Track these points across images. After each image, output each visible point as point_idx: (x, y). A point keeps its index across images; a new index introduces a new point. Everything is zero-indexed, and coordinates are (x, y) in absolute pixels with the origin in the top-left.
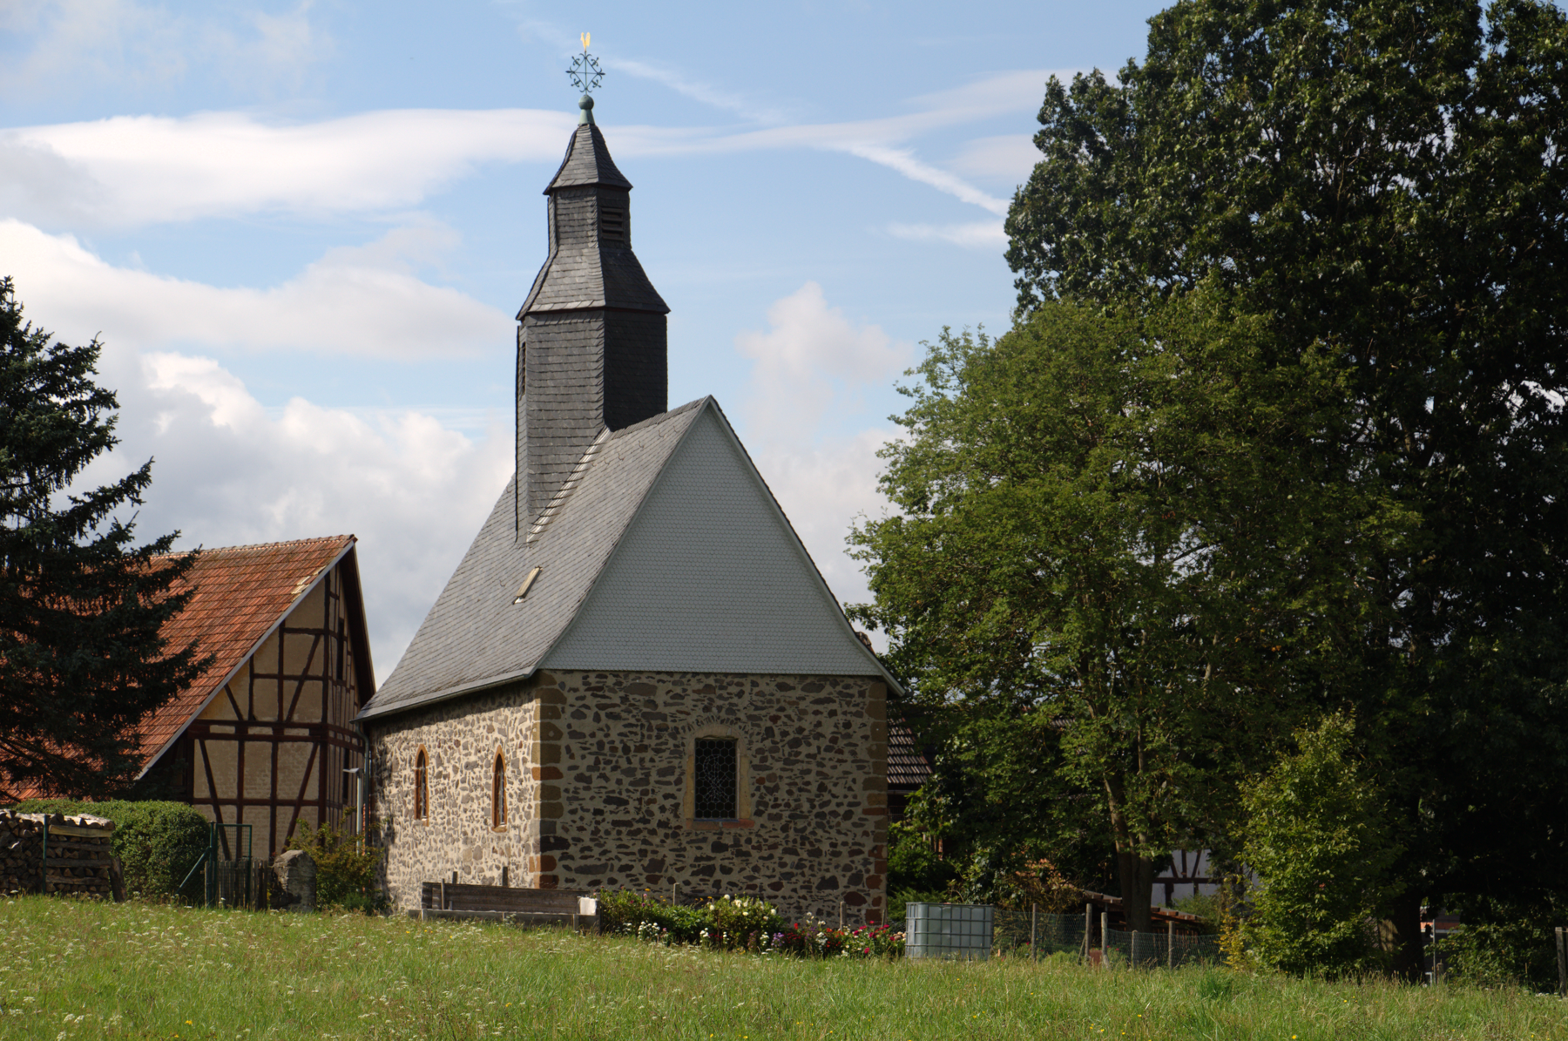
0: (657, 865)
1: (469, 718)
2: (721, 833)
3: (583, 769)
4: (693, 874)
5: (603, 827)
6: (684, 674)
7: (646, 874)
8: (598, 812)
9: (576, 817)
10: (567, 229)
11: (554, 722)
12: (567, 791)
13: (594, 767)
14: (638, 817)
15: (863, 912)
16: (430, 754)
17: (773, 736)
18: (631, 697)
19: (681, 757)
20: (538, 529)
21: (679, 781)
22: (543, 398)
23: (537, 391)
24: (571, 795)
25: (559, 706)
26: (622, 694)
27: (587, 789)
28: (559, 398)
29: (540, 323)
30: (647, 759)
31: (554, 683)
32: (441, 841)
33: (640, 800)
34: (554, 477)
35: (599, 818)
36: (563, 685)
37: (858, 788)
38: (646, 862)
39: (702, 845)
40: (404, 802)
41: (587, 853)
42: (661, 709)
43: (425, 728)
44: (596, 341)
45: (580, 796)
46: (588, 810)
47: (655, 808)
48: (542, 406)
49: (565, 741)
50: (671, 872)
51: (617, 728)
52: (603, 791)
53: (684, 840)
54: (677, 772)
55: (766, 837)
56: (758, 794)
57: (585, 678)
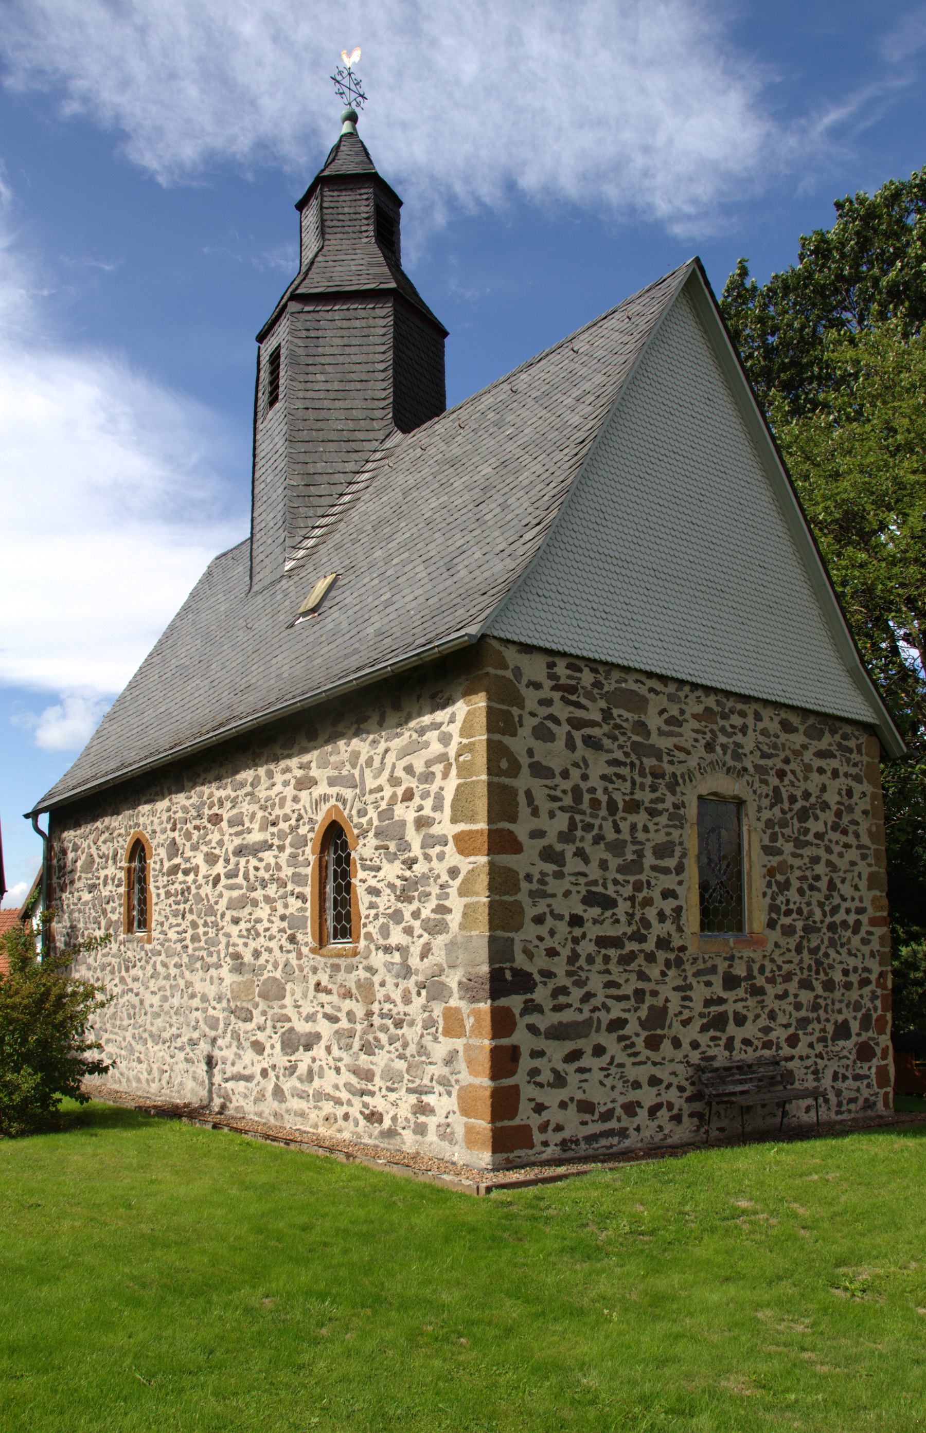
0: (658, 1017)
1: (246, 775)
2: (732, 958)
3: (551, 838)
4: (704, 1029)
5: (587, 948)
6: (681, 682)
7: (644, 1034)
8: (576, 921)
9: (543, 930)
10: (335, 223)
11: (507, 740)
12: (529, 877)
13: (566, 837)
14: (629, 931)
15: (873, 1070)
16: (154, 843)
17: (782, 802)
18: (615, 712)
19: (682, 827)
20: (301, 553)
21: (680, 869)
22: (310, 394)
23: (301, 386)
24: (535, 886)
25: (515, 711)
26: (603, 704)
27: (559, 875)
28: (332, 395)
29: (307, 309)
30: (640, 826)
31: (505, 666)
32: (178, 966)
33: (632, 899)
34: (323, 489)
35: (577, 932)
36: (517, 671)
37: (863, 885)
38: (643, 1013)
39: (711, 978)
40: (104, 912)
41: (562, 999)
42: (655, 740)
43: (145, 808)
44: (383, 331)
45: (549, 889)
46: (560, 917)
47: (651, 913)
48: (308, 404)
49: (523, 782)
50: (676, 1028)
51: (598, 767)
52: (582, 880)
53: (690, 969)
54: (678, 851)
55: (780, 963)
56: (769, 892)
57: (551, 666)
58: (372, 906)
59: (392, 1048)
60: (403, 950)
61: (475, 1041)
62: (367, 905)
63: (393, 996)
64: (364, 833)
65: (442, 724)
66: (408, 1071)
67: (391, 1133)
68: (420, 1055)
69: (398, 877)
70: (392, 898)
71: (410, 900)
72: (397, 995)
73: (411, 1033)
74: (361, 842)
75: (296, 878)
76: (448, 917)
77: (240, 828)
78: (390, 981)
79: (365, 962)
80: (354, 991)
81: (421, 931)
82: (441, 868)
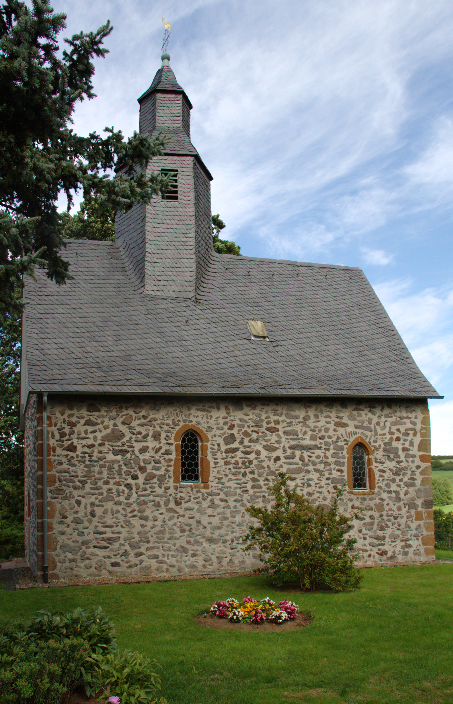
58: (381, 476)
59: (393, 527)
60: (397, 493)
61: (427, 521)
62: (378, 475)
63: (393, 508)
64: (377, 449)
65: (411, 418)
66: (401, 534)
67: (392, 557)
68: (406, 527)
69: (266, 457)
70: (391, 474)
71: (399, 475)
72: (395, 508)
73: (402, 521)
74: (376, 452)
75: (337, 463)
76: (416, 482)
77: (295, 437)
78: (391, 503)
79: (379, 497)
80: (374, 507)
81: (404, 486)
82: (413, 466)
